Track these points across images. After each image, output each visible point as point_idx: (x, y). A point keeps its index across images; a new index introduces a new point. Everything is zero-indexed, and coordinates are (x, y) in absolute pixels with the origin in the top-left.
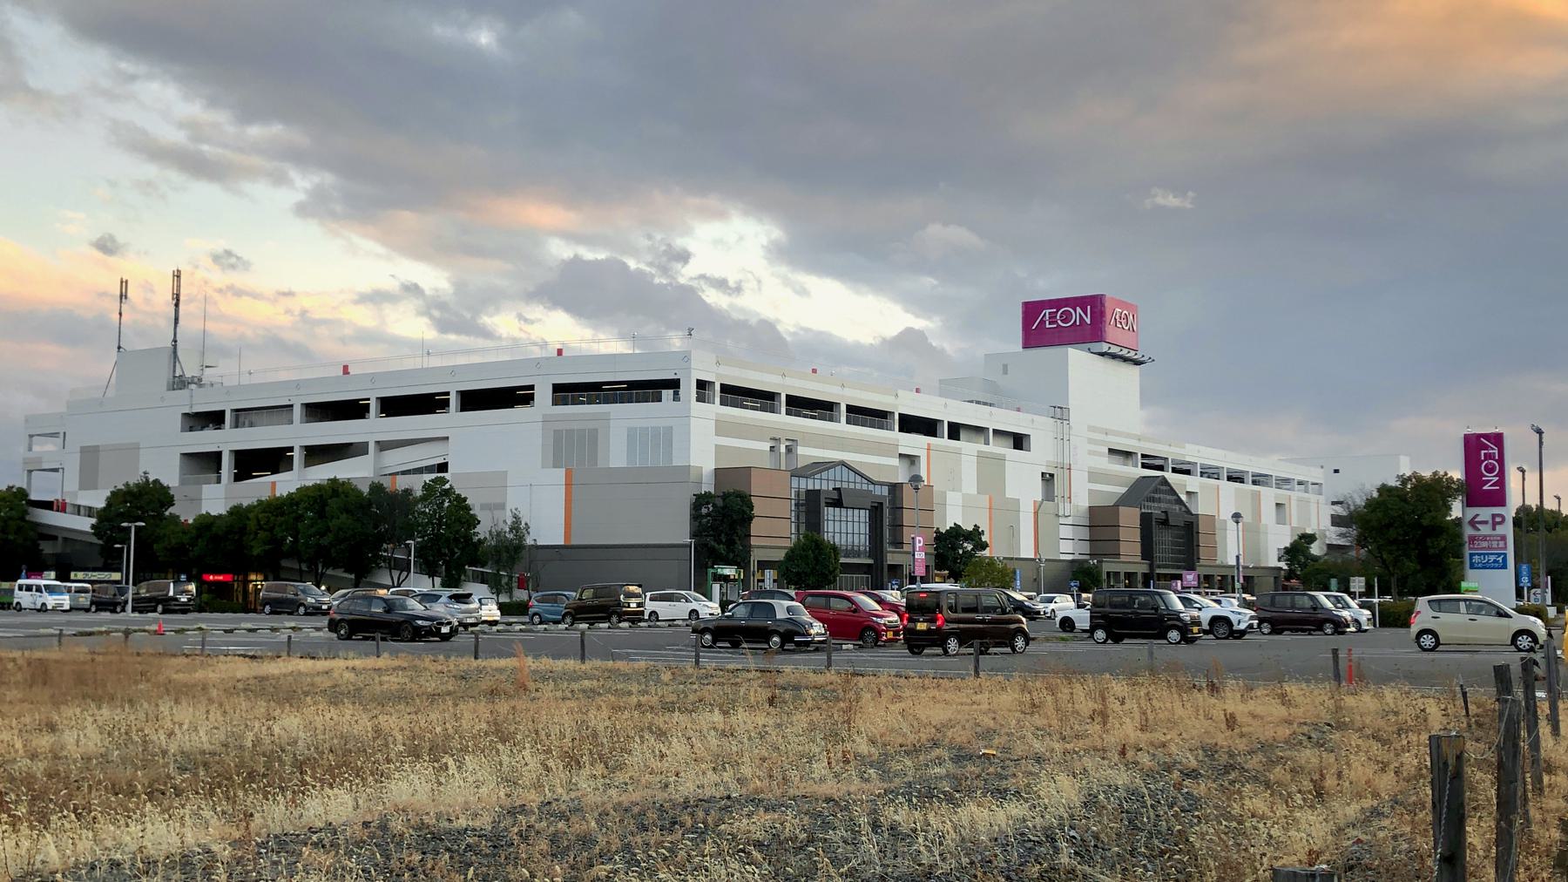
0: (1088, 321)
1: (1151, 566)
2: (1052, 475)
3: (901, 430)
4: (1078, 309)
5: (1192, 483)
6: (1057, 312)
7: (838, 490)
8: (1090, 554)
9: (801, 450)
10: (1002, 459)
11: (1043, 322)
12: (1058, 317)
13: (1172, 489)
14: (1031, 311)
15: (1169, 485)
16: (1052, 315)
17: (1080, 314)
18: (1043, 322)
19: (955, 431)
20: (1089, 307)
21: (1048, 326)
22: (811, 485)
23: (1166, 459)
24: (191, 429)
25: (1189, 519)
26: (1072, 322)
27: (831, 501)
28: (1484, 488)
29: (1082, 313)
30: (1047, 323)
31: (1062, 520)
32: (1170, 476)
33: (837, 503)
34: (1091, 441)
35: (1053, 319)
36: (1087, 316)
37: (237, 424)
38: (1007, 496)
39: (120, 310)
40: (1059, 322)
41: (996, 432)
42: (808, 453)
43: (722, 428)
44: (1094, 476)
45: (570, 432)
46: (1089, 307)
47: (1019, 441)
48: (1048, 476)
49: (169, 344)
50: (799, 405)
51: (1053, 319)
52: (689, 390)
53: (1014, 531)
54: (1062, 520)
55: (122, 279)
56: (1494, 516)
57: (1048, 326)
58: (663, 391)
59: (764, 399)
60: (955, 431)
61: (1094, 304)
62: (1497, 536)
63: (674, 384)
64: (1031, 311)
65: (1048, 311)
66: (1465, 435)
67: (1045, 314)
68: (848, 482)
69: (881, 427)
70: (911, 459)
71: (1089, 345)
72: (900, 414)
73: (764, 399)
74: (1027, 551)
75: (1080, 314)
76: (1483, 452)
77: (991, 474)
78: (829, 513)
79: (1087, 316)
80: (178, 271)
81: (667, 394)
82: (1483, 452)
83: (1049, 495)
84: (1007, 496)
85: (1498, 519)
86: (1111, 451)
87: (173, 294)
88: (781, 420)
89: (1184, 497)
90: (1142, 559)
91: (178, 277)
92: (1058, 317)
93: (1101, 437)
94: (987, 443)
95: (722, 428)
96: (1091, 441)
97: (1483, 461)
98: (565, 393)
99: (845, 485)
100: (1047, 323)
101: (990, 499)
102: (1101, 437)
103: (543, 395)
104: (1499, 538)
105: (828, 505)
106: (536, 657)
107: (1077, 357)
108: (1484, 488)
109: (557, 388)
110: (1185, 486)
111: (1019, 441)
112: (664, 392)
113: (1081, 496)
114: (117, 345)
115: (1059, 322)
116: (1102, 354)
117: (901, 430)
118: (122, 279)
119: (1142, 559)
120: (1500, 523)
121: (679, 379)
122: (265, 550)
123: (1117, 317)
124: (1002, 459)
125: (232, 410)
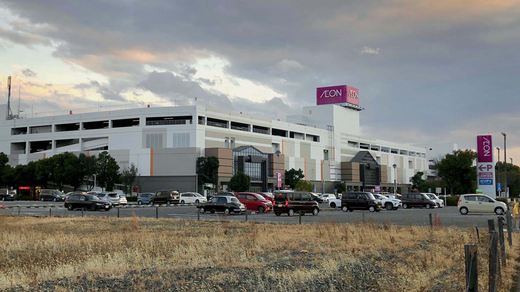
1: (364, 184)
2: (327, 151)
5: (378, 153)
6: (329, 91)
7: (250, 156)
9: (236, 142)
10: (309, 145)
11: (324, 95)
12: (330, 94)
14: (320, 91)
16: (328, 93)
17: (338, 92)
18: (324, 95)
19: (292, 135)
20: (341, 90)
21: (326, 97)
24: (15, 134)
25: (377, 166)
26: (335, 95)
30: (326, 95)
31: (331, 167)
33: (249, 161)
34: (342, 138)
37: (31, 132)
40: (330, 95)
41: (307, 135)
42: (239, 143)
43: (208, 134)
44: (343, 151)
45: (152, 135)
47: (315, 138)
48: (326, 151)
50: (235, 125)
52: (196, 120)
54: (331, 167)
56: (488, 166)
57: (326, 97)
59: (223, 123)
60: (292, 135)
61: (343, 89)
62: (489, 173)
63: (190, 118)
64: (320, 91)
66: (477, 136)
70: (276, 145)
73: (223, 123)
77: (305, 151)
78: (247, 164)
81: (188, 121)
83: (326, 158)
84: (311, 158)
85: (489, 167)
86: (349, 142)
88: (229, 131)
90: (360, 181)
92: (330, 94)
95: (208, 134)
96: (342, 138)
98: (151, 121)
99: (252, 154)
100: (326, 95)
103: (143, 122)
104: (490, 174)
105: (246, 161)
107: (336, 108)
109: (148, 119)
110: (376, 154)
111: (315, 138)
112: (187, 121)
113: (338, 158)
115: (330, 95)
116: (346, 107)
119: (360, 181)
120: (490, 168)
123: (351, 94)
124: (309, 145)
125: (30, 127)
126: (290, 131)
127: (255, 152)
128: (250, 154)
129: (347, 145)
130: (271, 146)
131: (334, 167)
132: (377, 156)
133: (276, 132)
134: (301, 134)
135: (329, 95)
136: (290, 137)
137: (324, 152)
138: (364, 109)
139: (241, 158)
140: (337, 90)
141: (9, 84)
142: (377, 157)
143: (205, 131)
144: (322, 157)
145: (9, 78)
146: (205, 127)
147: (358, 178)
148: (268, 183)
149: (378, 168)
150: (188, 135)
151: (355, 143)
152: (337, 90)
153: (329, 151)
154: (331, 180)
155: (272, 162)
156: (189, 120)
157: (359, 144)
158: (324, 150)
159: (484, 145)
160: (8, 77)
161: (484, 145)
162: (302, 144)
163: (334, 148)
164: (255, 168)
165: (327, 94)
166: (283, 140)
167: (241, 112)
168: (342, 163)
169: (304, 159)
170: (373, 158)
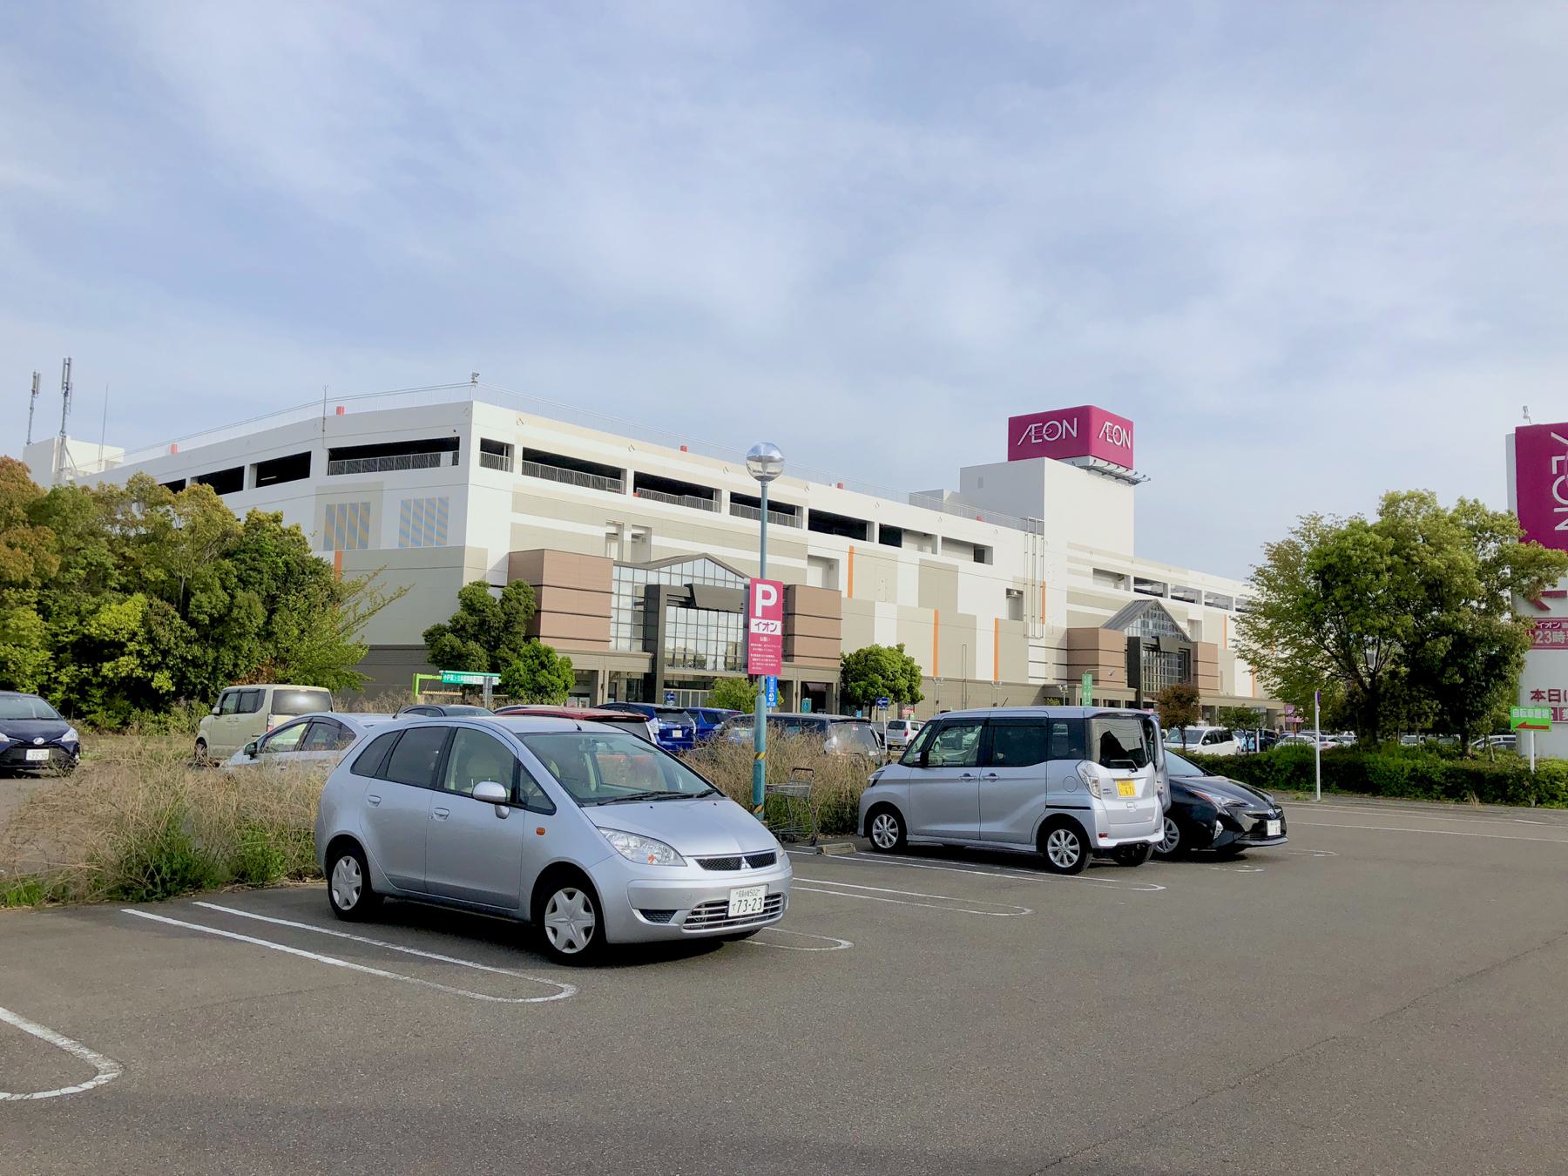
0: (1074, 434)
1: (1138, 694)
2: (1020, 593)
3: (881, 541)
4: (1065, 423)
5: (1195, 611)
6: (1043, 426)
7: (690, 586)
8: (1067, 680)
9: (656, 540)
10: (954, 571)
11: (1029, 437)
12: (1044, 431)
13: (1168, 615)
14: (1017, 426)
15: (1163, 610)
16: (1039, 431)
17: (1066, 428)
18: (1029, 437)
19: (891, 536)
20: (1075, 419)
21: (1033, 441)
22: (653, 578)
23: (1165, 585)
25: (1187, 646)
26: (1059, 434)
27: (683, 600)
28: (1557, 528)
29: (1069, 428)
30: (1033, 437)
31: (1031, 642)
32: (1166, 602)
33: (689, 603)
34: (1071, 559)
35: (1039, 435)
36: (1073, 429)
38: (960, 611)
39: (32, 404)
40: (1045, 437)
41: (945, 540)
42: (662, 544)
43: (521, 502)
44: (1074, 597)
45: (342, 507)
46: (1075, 419)
47: (980, 554)
48: (1015, 593)
49: (1055, 650)
51: (1039, 435)
52: (474, 452)
53: (966, 651)
54: (1031, 642)
55: (35, 373)
57: (1033, 441)
58: (442, 453)
59: (603, 475)
60: (891, 536)
61: (1082, 416)
63: (451, 445)
64: (1017, 426)
65: (1034, 426)
66: (1518, 429)
67: (1031, 429)
68: (715, 579)
69: (792, 525)
70: (829, 564)
71: (1075, 459)
72: (810, 511)
73: (603, 475)
74: (984, 672)
75: (1066, 428)
76: (1555, 459)
77: (937, 588)
78: (672, 615)
79: (1073, 429)
80: (70, 359)
81: (446, 456)
82: (1555, 459)
83: (1017, 613)
84: (960, 611)
86: (1097, 572)
87: (63, 383)
88: (628, 502)
89: (1183, 625)
90: (1129, 687)
91: (68, 364)
92: (1044, 431)
93: (1087, 556)
94: (934, 552)
95: (521, 502)
96: (1071, 559)
97: (1557, 477)
98: (343, 457)
99: (697, 581)
100: (1033, 437)
101: (936, 612)
102: (1087, 556)
103: (319, 463)
105: (670, 603)
106: (1282, 747)
107: (1053, 469)
108: (1557, 528)
110: (1187, 613)
111: (980, 554)
113: (1058, 618)
114: (26, 441)
115: (1045, 437)
116: (1089, 468)
117: (881, 541)
118: (35, 373)
119: (1129, 687)
121: (458, 438)
122: (1195, 725)
123: (1107, 431)
124: (954, 571)
126: (880, 525)
127: (709, 574)
128: (688, 581)
129: (1092, 579)
130: (803, 564)
131: (1042, 642)
132: (1189, 618)
133: (823, 522)
134: (926, 537)
135: (1042, 437)
136: (880, 542)
137: (1007, 597)
138: (1149, 479)
139: (652, 593)
140: (1064, 421)
141: (66, 381)
142: (1191, 622)
143: (511, 494)
144: (1002, 608)
145: (67, 362)
146: (514, 477)
147: (1122, 675)
148: (1144, 703)
149: (1189, 650)
150: (444, 502)
151: (1120, 577)
152: (1064, 421)
153: (1025, 594)
154: (1031, 681)
155: (792, 612)
156: (450, 454)
157: (1132, 580)
158: (1009, 592)
159: (1555, 471)
160: (65, 360)
161: (1555, 471)
162: (923, 565)
163: (1043, 587)
164: (715, 629)
165: (1035, 433)
166: (852, 548)
167: (682, 447)
168: (1070, 633)
169: (933, 611)
170: (1173, 621)
